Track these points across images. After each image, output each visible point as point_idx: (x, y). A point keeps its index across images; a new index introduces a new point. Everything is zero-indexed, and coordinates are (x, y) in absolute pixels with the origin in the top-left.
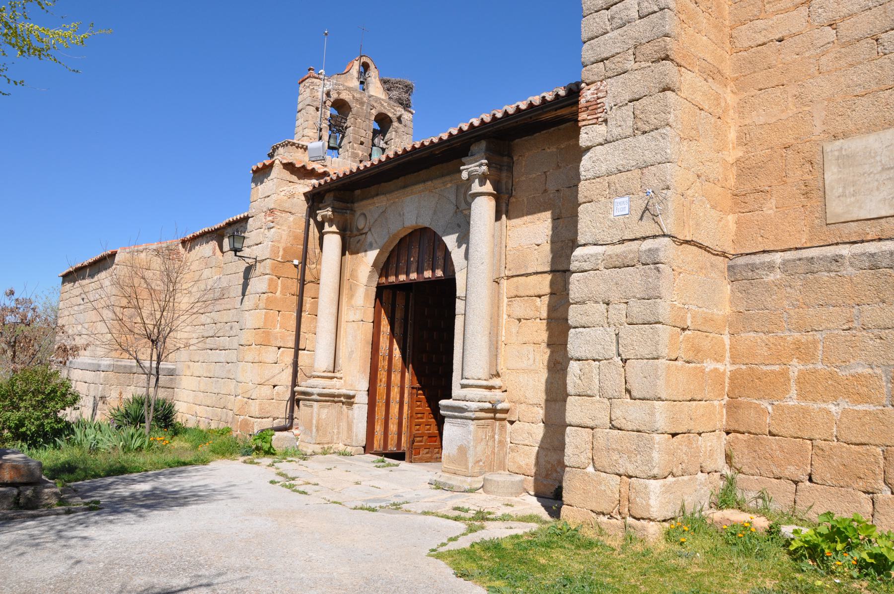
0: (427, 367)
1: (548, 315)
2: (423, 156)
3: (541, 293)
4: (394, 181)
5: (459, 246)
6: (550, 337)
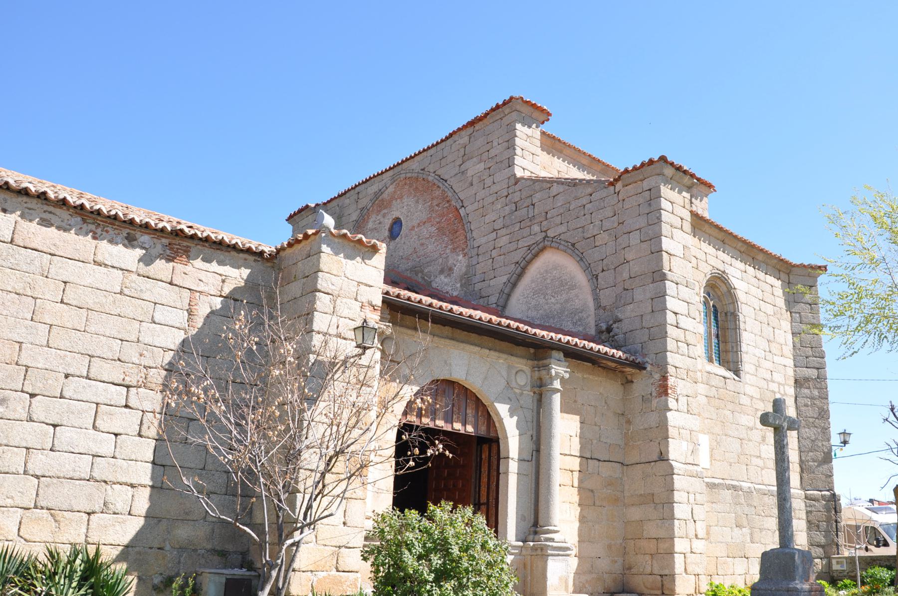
0: (445, 493)
1: (579, 485)
2: (482, 326)
3: (574, 469)
4: (439, 326)
5: (511, 416)
6: (580, 499)
